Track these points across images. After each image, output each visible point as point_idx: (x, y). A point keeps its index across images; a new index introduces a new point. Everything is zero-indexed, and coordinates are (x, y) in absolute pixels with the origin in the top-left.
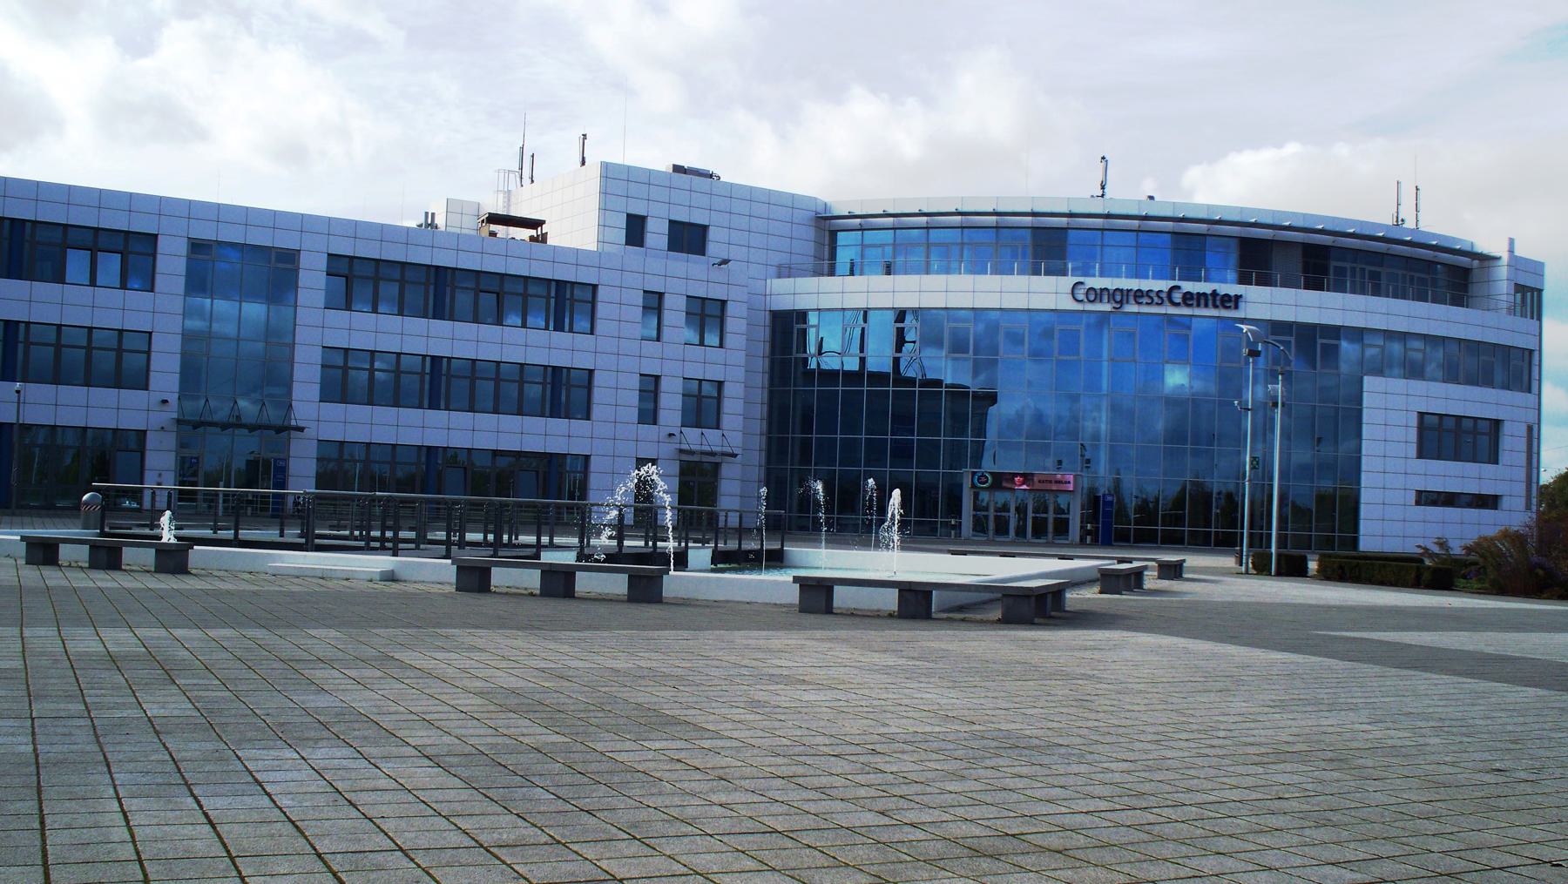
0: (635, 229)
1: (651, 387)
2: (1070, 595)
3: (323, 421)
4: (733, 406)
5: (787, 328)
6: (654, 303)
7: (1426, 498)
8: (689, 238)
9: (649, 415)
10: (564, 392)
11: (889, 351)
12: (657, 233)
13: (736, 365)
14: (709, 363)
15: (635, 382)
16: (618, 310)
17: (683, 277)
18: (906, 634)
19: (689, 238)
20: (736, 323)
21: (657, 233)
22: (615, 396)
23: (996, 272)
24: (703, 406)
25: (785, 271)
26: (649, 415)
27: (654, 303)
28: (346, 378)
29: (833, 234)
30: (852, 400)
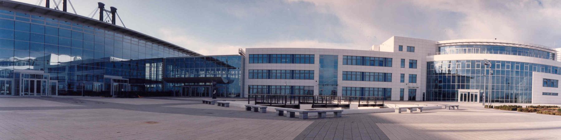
0: (401, 48)
1: (403, 76)
2: (309, 114)
3: (342, 84)
4: (418, 79)
5: (430, 65)
6: (403, 61)
7: (544, 94)
8: (411, 49)
9: (403, 81)
10: (386, 77)
11: (155, 77)
12: (405, 49)
13: (420, 72)
14: (413, 71)
15: (400, 75)
16: (396, 63)
17: (409, 57)
18: (293, 122)
19: (411, 49)
20: (419, 64)
21: (405, 49)
22: (396, 78)
23: (495, 53)
24: (413, 78)
25: (429, 54)
26: (403, 81)
27: (403, 61)
28: (347, 76)
29: (439, 48)
30: (440, 77)
